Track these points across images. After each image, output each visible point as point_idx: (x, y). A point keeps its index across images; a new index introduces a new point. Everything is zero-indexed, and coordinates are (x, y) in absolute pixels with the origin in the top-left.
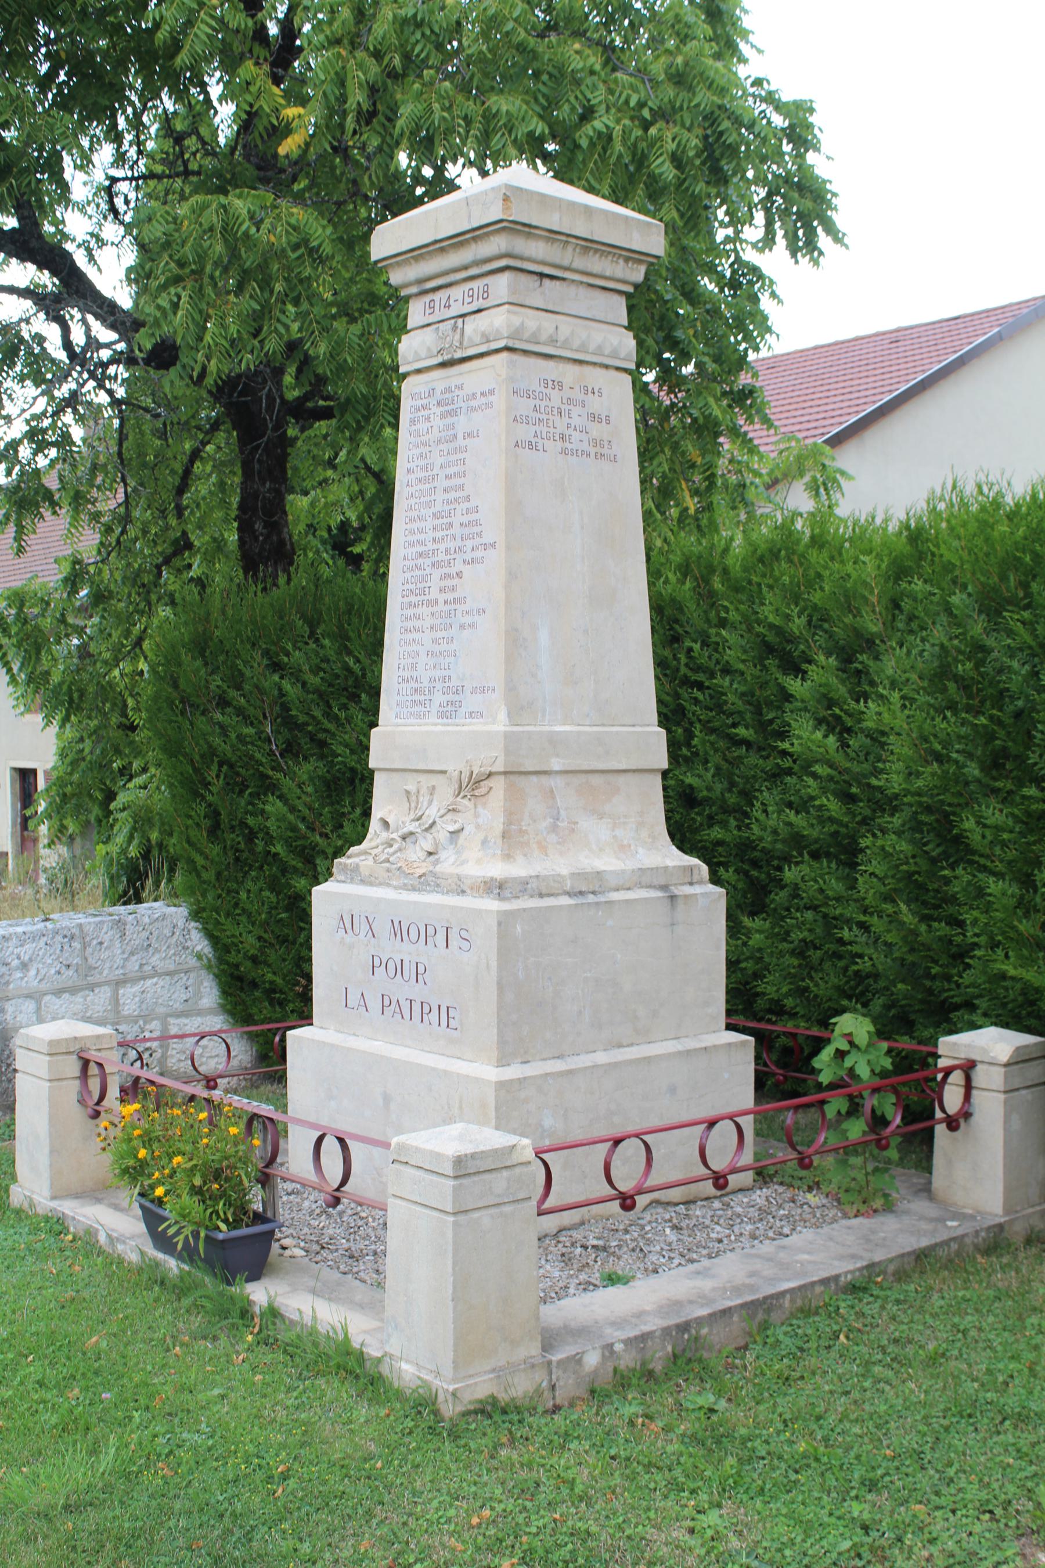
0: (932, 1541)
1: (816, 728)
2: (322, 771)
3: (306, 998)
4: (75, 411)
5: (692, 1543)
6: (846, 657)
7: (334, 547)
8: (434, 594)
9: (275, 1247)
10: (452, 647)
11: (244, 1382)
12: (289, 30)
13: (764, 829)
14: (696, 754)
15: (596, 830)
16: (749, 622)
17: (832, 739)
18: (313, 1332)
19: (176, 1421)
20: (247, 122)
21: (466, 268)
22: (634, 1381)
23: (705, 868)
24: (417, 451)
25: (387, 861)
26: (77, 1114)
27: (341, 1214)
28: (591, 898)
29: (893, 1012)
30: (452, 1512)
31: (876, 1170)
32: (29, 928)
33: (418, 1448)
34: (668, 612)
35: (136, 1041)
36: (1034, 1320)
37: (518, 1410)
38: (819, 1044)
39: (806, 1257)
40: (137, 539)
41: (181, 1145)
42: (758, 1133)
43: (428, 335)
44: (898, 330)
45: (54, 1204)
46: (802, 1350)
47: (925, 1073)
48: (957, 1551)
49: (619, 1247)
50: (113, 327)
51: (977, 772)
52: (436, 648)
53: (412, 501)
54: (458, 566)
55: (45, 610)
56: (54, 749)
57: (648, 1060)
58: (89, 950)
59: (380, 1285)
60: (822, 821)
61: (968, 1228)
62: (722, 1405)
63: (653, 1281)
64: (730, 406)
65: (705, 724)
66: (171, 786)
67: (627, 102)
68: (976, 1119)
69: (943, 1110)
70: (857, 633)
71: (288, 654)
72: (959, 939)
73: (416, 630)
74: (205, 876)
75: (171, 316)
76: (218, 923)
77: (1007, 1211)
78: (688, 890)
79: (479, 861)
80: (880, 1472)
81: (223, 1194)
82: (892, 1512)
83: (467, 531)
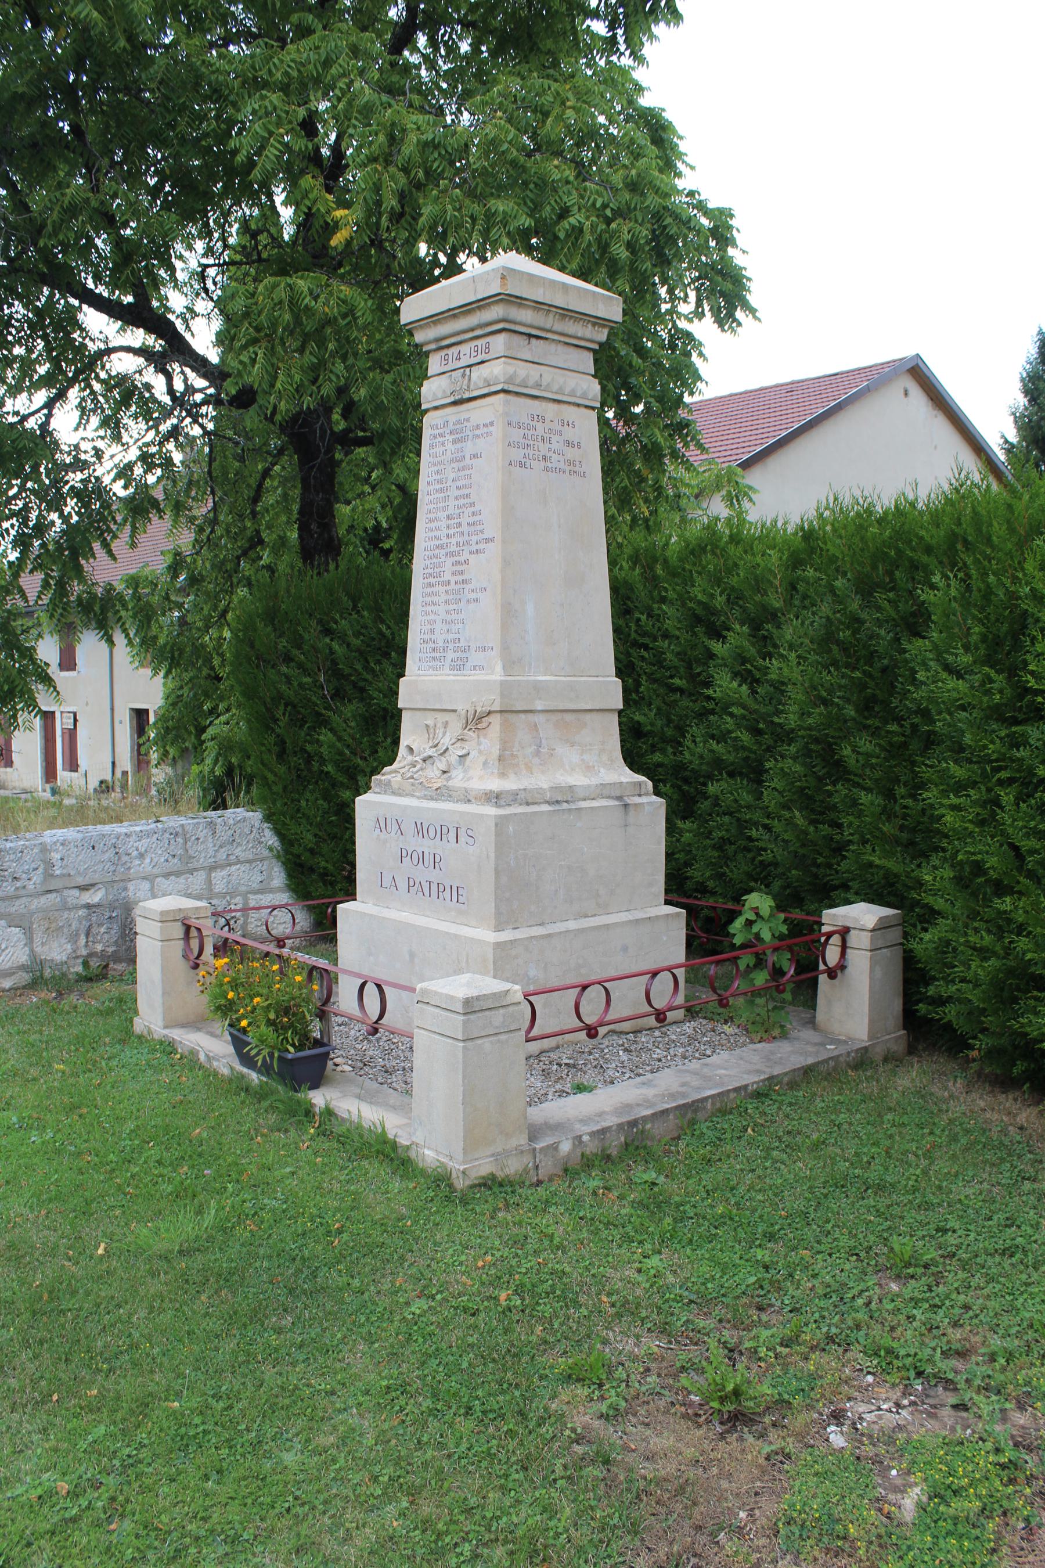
0: (815, 1276)
1: (733, 679)
2: (362, 710)
3: (351, 879)
4: (176, 440)
5: (640, 1279)
6: (756, 626)
7: (370, 543)
8: (447, 576)
9: (330, 1063)
10: (461, 616)
11: (308, 1163)
12: (337, 150)
13: (693, 755)
14: (643, 698)
15: (571, 755)
16: (683, 599)
17: (744, 687)
18: (359, 1126)
19: (259, 1190)
20: (306, 222)
21: (472, 330)
22: (597, 1163)
23: (650, 784)
24: (435, 469)
25: (412, 777)
26: (181, 966)
27: (378, 1040)
28: (565, 806)
29: (788, 891)
30: (463, 1258)
31: (775, 1008)
32: (145, 828)
33: (438, 1212)
34: (622, 591)
35: (224, 911)
36: (889, 1116)
37: (511, 1184)
38: (733, 915)
39: (723, 1071)
40: (222, 536)
41: (259, 989)
42: (687, 981)
43: (443, 381)
44: (792, 383)
45: (166, 1032)
46: (720, 1139)
47: (813, 937)
48: (833, 1283)
49: (585, 1064)
50: (204, 376)
51: (853, 713)
52: (449, 617)
53: (431, 506)
54: (466, 555)
55: (154, 590)
56: (161, 695)
57: (607, 926)
58: (189, 844)
59: (408, 1093)
60: (736, 749)
61: (842, 1050)
62: (661, 1179)
63: (610, 1089)
64: (670, 435)
65: (649, 676)
66: (249, 721)
67: (594, 204)
68: (850, 970)
69: (825, 963)
70: (764, 607)
71: (336, 623)
72: (838, 837)
73: (434, 604)
74: (275, 788)
75: (249, 368)
76: (284, 824)
77: (870, 1038)
78: (637, 800)
79: (481, 778)
80: (777, 1227)
81: (291, 1025)
82: (786, 1256)
83: (472, 529)
